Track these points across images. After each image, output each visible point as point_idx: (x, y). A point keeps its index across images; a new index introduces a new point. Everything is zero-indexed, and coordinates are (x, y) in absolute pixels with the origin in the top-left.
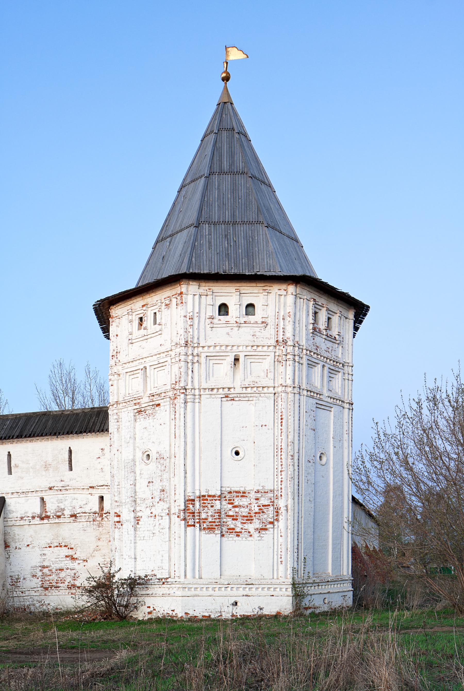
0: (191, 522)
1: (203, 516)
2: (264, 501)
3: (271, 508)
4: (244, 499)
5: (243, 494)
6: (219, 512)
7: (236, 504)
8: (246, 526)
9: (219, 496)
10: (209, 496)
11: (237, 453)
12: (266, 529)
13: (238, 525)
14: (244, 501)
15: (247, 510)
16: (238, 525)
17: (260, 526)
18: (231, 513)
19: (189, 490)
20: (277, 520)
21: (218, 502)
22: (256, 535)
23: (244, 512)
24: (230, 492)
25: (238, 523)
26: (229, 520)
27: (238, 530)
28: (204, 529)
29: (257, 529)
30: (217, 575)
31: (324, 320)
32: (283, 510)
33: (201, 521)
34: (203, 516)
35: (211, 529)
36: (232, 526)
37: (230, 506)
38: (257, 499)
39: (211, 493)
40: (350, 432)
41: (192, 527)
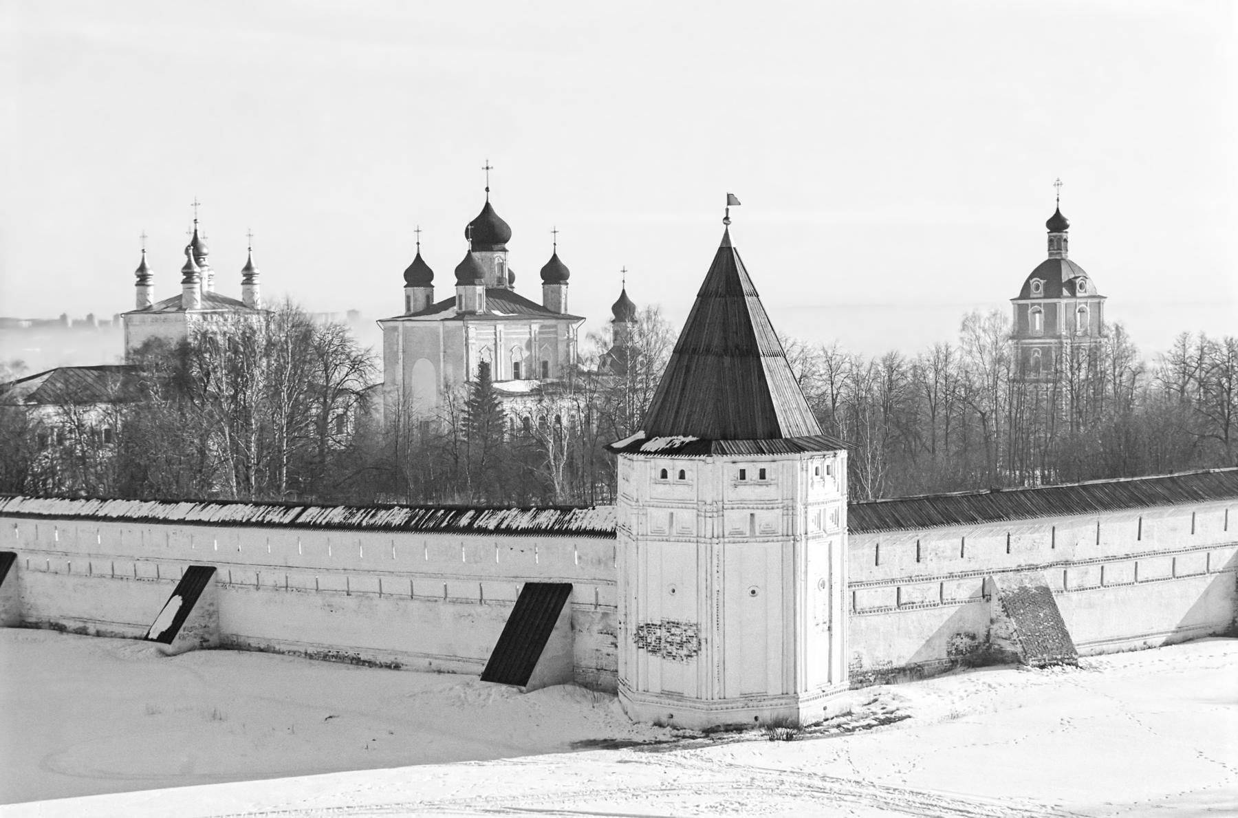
0: (641, 645)
1: (649, 641)
2: (690, 633)
3: (695, 639)
4: (678, 629)
5: (677, 625)
6: (660, 639)
7: (672, 632)
8: (680, 652)
9: (660, 626)
10: (653, 625)
11: (753, 592)
12: (691, 656)
13: (673, 649)
14: (678, 631)
15: (679, 638)
16: (673, 649)
17: (688, 653)
18: (669, 640)
19: (641, 617)
20: (700, 650)
21: (658, 630)
22: (685, 658)
23: (678, 639)
24: (668, 623)
25: (674, 648)
26: (668, 645)
27: (674, 654)
28: (650, 651)
29: (685, 655)
30: (1069, 571)
31: (969, 580)
32: (703, 642)
33: (648, 644)
34: (649, 641)
35: (654, 652)
36: (670, 651)
37: (668, 634)
38: (685, 631)
39: (654, 623)
40: (578, 582)
41: (981, 594)
